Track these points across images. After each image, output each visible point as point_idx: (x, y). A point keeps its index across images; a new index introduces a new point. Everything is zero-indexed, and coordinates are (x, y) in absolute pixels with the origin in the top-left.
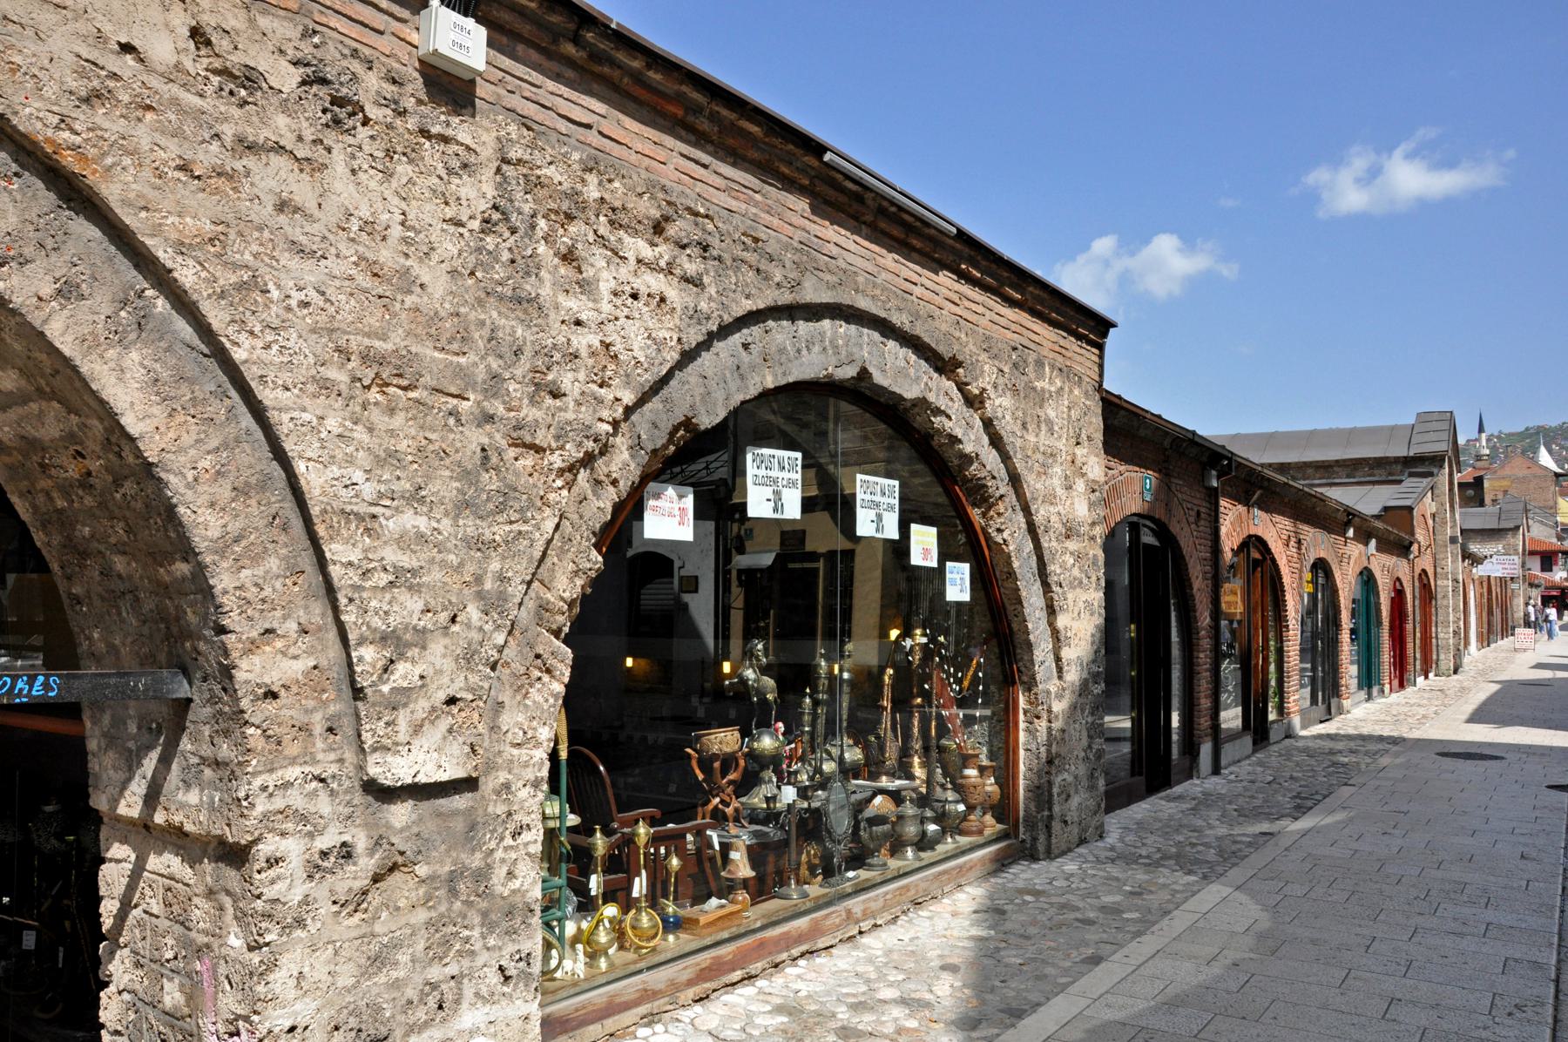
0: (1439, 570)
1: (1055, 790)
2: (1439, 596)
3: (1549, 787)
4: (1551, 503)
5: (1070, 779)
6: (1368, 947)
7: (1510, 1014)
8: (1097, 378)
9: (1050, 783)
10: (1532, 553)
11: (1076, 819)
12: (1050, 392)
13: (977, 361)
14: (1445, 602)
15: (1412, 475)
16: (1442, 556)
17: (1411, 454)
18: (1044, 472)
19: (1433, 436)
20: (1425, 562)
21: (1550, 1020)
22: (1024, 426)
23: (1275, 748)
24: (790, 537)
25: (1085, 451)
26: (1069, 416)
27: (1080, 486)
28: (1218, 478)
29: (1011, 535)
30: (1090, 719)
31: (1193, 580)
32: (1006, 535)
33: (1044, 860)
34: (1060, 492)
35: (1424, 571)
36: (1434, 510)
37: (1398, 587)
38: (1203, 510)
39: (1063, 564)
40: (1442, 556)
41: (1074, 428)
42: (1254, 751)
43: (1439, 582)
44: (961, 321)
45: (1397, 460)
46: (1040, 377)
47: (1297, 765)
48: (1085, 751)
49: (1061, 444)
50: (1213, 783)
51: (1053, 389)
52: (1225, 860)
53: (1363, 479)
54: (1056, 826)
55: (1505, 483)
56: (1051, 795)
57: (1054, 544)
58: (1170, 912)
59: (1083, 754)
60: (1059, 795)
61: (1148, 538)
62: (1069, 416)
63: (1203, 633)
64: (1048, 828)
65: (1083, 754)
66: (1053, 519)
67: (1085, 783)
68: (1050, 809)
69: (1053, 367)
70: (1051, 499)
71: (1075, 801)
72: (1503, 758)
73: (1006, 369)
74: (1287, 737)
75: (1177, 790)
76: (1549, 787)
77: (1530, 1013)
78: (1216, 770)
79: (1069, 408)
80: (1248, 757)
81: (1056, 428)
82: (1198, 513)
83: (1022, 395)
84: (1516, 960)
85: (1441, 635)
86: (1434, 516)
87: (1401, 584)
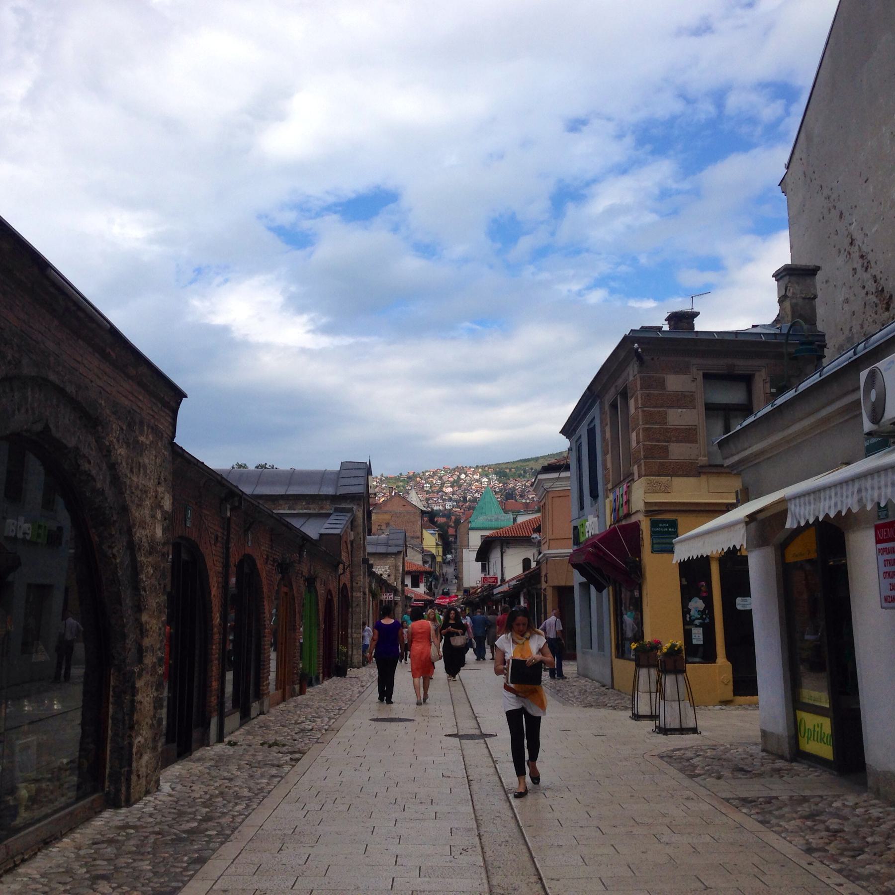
0: (354, 584)
1: (134, 750)
2: (354, 605)
3: (446, 735)
4: (419, 534)
5: (142, 741)
6: (373, 832)
7: (461, 854)
8: (171, 434)
9: (131, 745)
10: (409, 573)
11: (145, 774)
12: (146, 445)
13: (109, 421)
14: (358, 610)
15: (337, 510)
16: (357, 574)
17: (338, 494)
18: (139, 506)
19: (353, 481)
20: (345, 579)
21: (481, 853)
22: (132, 471)
23: (255, 721)
24: (480, 600)
25: (163, 489)
26: (156, 463)
27: (159, 516)
28: (231, 510)
29: (118, 551)
30: (155, 694)
31: (212, 587)
32: (115, 550)
33: (124, 807)
34: (148, 519)
35: (344, 584)
36: (352, 538)
37: (329, 597)
38: (219, 534)
39: (148, 577)
40: (357, 574)
41: (157, 472)
42: (241, 725)
43: (354, 594)
44: (102, 391)
45: (326, 497)
46: (142, 434)
47: (276, 732)
48: (151, 719)
49: (150, 484)
50: (219, 748)
51: (148, 443)
52: (256, 795)
53: (301, 511)
54: (134, 778)
55: (387, 517)
56: (131, 754)
57: (143, 558)
58: (237, 828)
59: (150, 722)
60: (136, 754)
61: (184, 556)
62: (156, 463)
63: (215, 630)
64: (128, 781)
65: (150, 722)
66: (144, 540)
67: (151, 745)
68: (130, 765)
69: (148, 427)
70: (143, 525)
71: (146, 758)
72: (413, 720)
73: (124, 428)
74: (260, 714)
75: (197, 754)
76: (446, 735)
77: (470, 852)
78: (220, 740)
79: (156, 457)
80: (237, 729)
81: (148, 472)
82: (217, 537)
83: (132, 447)
84: (457, 829)
85: (355, 635)
86: (352, 542)
87: (332, 597)
